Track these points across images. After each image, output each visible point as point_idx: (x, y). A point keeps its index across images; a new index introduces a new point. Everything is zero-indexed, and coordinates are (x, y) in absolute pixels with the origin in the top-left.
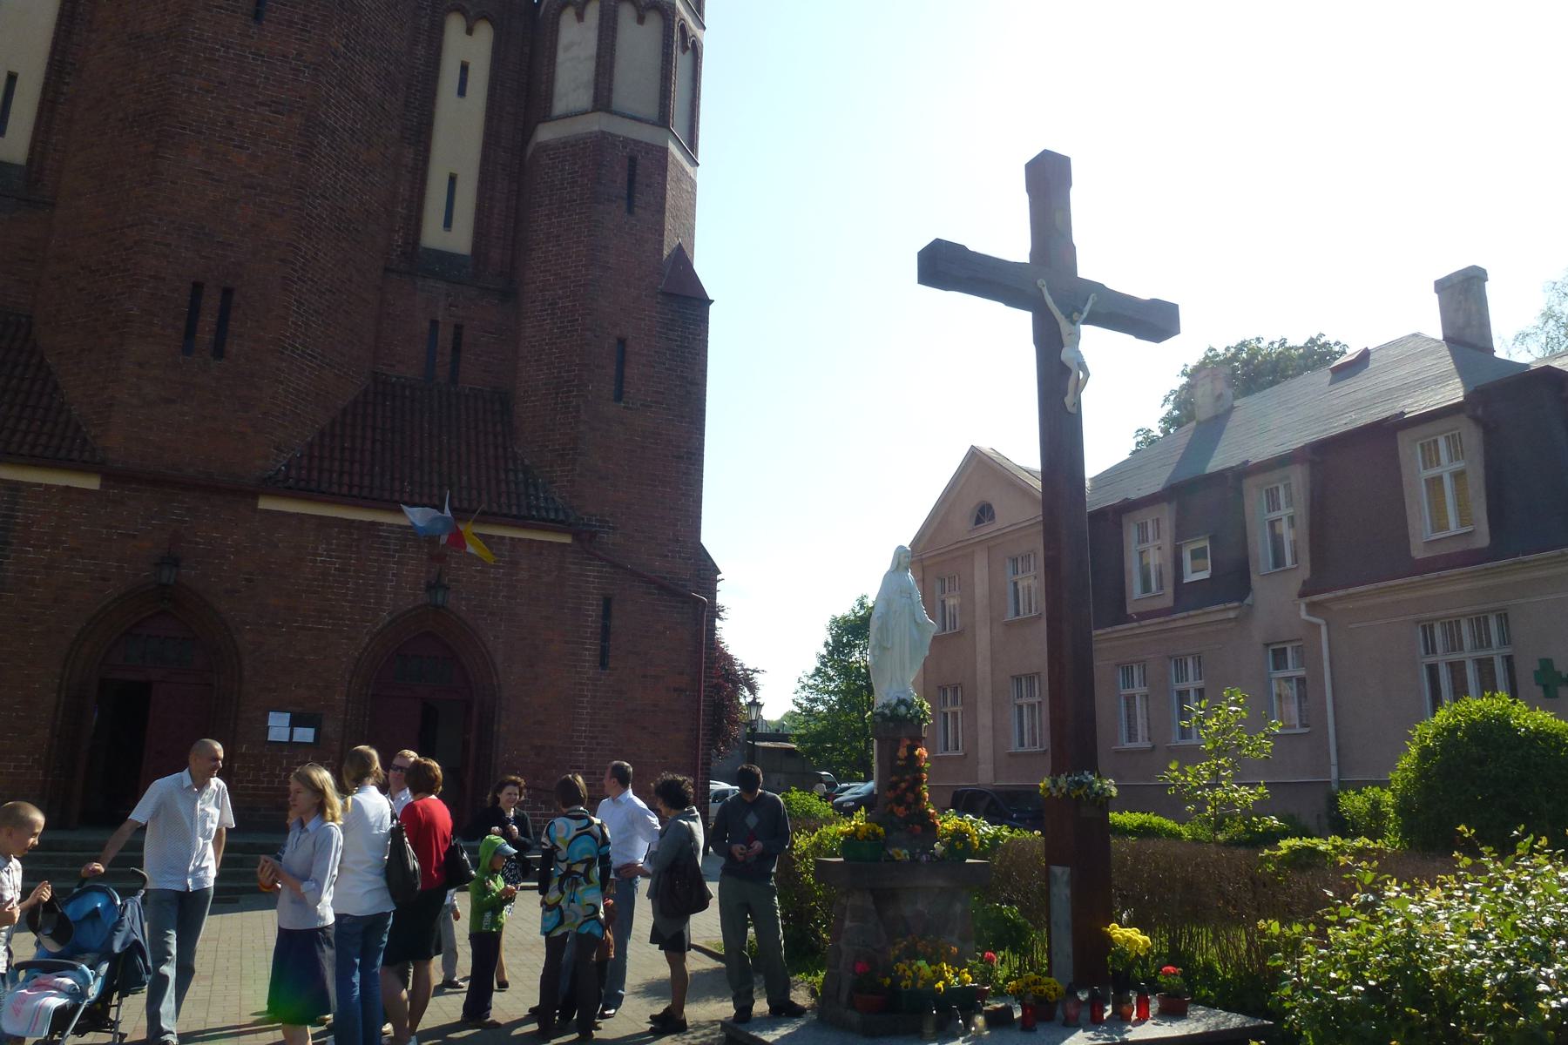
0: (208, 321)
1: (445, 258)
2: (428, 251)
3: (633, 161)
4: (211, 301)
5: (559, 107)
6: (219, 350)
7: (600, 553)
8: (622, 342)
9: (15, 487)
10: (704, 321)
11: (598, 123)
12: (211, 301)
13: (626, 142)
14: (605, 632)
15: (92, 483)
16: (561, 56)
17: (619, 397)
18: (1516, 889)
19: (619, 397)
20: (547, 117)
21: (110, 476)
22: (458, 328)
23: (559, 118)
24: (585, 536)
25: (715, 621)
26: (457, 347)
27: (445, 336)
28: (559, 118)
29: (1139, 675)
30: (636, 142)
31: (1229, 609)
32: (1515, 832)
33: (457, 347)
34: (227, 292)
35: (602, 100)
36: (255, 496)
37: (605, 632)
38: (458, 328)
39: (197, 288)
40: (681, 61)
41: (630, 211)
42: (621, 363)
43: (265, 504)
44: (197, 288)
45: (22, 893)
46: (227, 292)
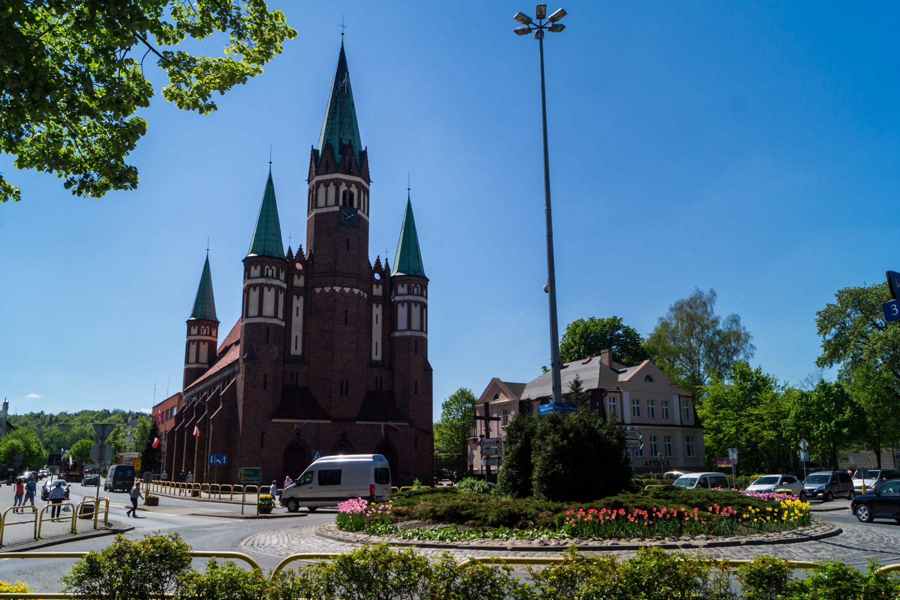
0: (344, 389)
1: (377, 362)
2: (374, 361)
3: (416, 341)
4: (345, 384)
5: (399, 328)
6: (347, 395)
8: (416, 382)
9: (319, 424)
10: (431, 374)
12: (345, 384)
15: (330, 422)
16: (399, 315)
17: (416, 393)
19: (416, 393)
21: (333, 420)
23: (399, 331)
25: (381, 276)
27: (379, 380)
28: (399, 331)
29: (204, 506)
31: (343, 490)
34: (347, 382)
39: (342, 382)
40: (425, 310)
41: (416, 352)
42: (416, 386)
43: (357, 422)
44: (342, 382)
46: (347, 382)
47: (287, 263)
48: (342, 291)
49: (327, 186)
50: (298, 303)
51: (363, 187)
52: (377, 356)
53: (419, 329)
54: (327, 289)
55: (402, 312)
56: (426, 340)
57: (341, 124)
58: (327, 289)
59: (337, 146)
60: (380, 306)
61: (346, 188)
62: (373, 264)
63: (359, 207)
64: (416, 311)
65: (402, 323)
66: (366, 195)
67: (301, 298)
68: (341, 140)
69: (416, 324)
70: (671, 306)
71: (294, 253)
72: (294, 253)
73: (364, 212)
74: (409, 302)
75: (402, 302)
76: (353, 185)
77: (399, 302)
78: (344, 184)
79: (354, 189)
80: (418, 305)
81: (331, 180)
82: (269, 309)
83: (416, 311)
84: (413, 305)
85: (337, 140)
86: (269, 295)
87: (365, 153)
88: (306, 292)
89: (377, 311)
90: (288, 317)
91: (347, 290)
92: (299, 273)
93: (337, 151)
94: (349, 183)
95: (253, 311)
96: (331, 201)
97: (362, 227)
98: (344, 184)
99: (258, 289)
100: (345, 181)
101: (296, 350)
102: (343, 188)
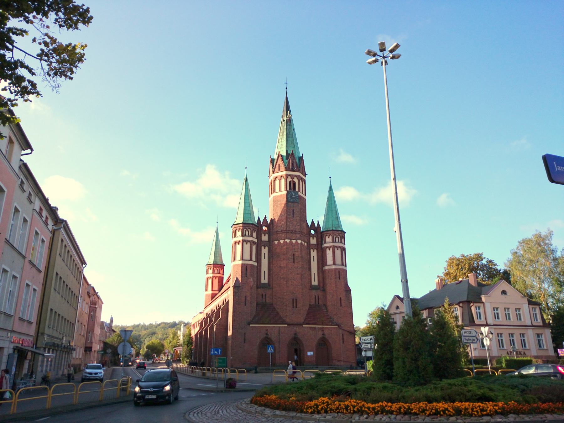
4: (295, 301)
7: (271, 260)
8: (341, 298)
11: (334, 267)
12: (295, 301)
13: (338, 269)
14: (343, 339)
15: (286, 326)
16: (327, 256)
17: (341, 306)
18: (376, 410)
19: (341, 306)
20: (326, 265)
21: (289, 324)
22: (318, 296)
24: (339, 326)
26: (318, 299)
30: (339, 269)
32: (442, 344)
33: (318, 299)
34: (296, 299)
35: (334, 264)
36: (303, 325)
37: (343, 339)
38: (318, 296)
39: (293, 299)
44: (293, 299)
45: (489, 402)
46: (296, 299)
50: (265, 251)
51: (302, 178)
54: (282, 241)
55: (329, 253)
58: (282, 241)
61: (291, 180)
66: (303, 183)
67: (267, 248)
69: (338, 261)
71: (262, 221)
72: (262, 221)
73: (303, 193)
76: (295, 178)
77: (327, 247)
79: (296, 180)
80: (339, 249)
83: (338, 252)
88: (269, 244)
89: (314, 254)
90: (259, 260)
92: (265, 232)
98: (289, 177)
99: (331, 249)
102: (289, 179)
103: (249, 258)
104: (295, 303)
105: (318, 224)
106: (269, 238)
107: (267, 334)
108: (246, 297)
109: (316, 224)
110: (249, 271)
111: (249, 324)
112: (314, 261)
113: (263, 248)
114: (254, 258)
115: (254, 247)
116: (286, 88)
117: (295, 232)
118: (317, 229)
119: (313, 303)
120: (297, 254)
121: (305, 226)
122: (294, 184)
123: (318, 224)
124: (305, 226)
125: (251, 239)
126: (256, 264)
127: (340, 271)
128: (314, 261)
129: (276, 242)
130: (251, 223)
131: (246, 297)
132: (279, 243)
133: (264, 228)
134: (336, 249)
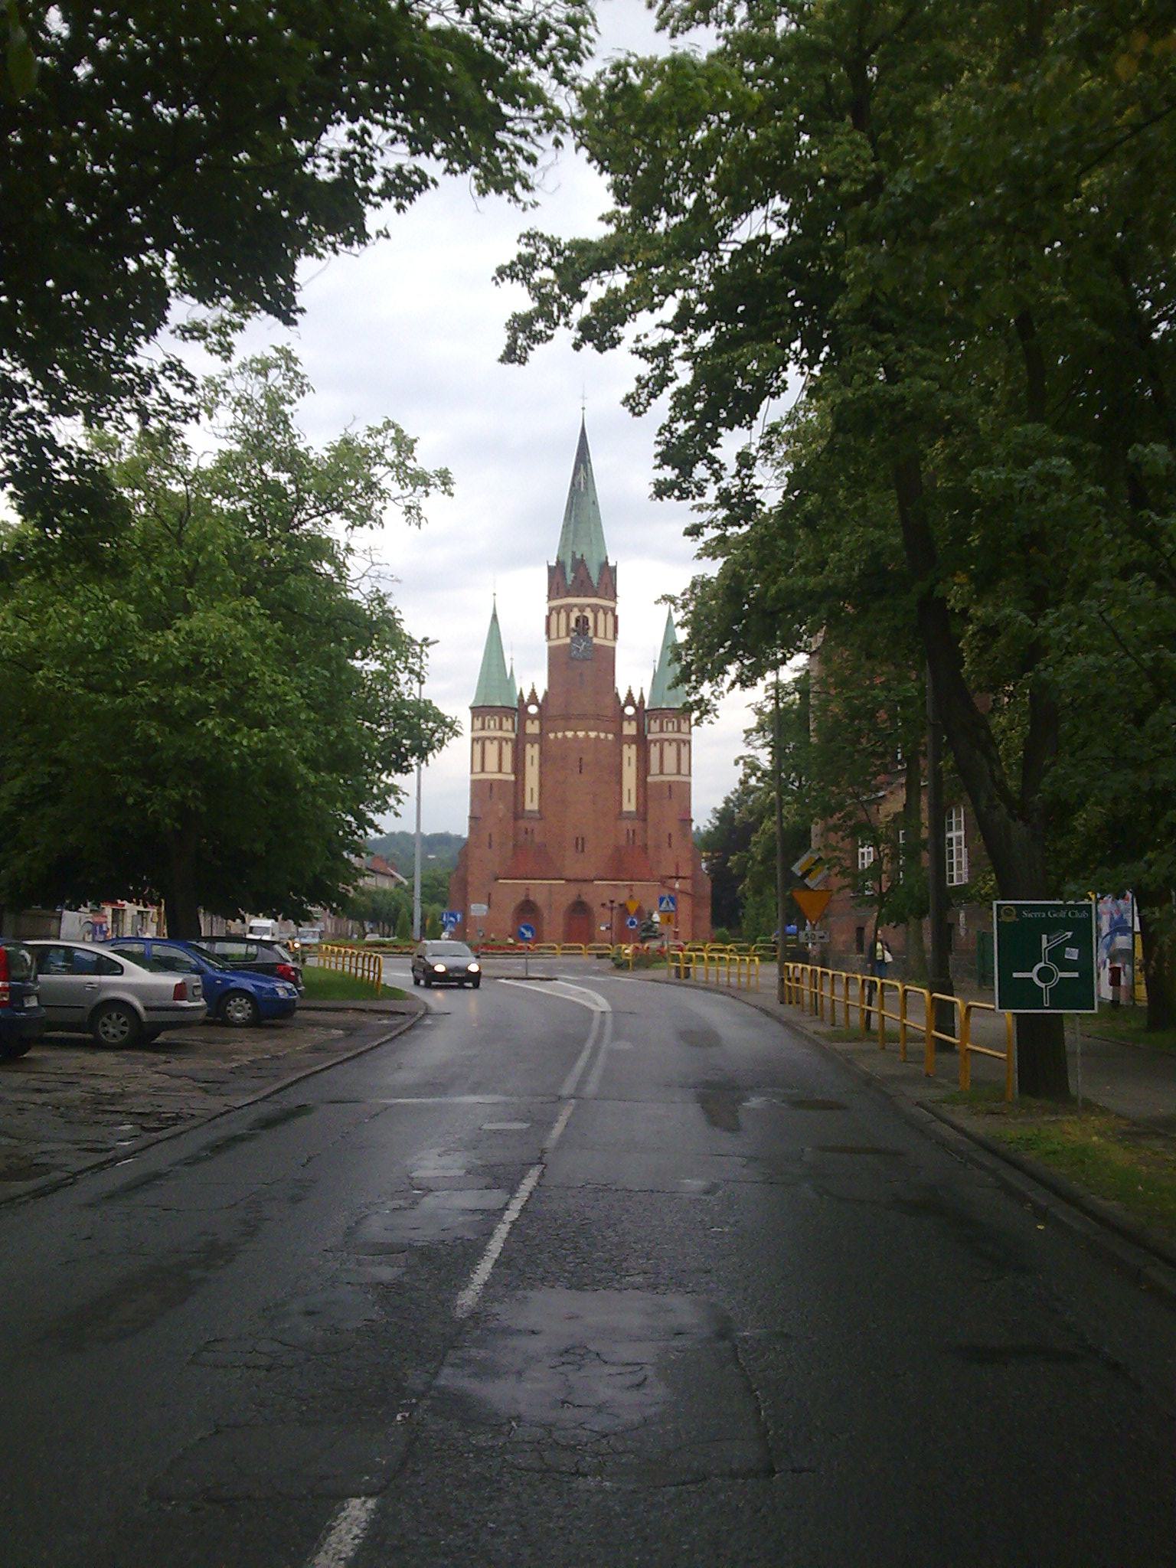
5: (652, 772)
35: (661, 773)
47: (518, 711)
48: (576, 737)
49: (558, 613)
50: (532, 752)
52: (630, 805)
53: (675, 771)
54: (560, 735)
55: (654, 751)
56: (689, 784)
57: (575, 536)
58: (560, 735)
59: (569, 563)
60: (634, 747)
61: (578, 614)
62: (623, 697)
63: (596, 635)
64: (670, 752)
65: (654, 767)
67: (536, 746)
68: (574, 553)
70: (657, 57)
71: (526, 698)
72: (526, 698)
74: (662, 741)
75: (655, 741)
76: (588, 609)
77: (652, 741)
78: (576, 609)
79: (589, 614)
81: (562, 607)
82: (492, 763)
84: (504, 744)
85: (570, 554)
86: (492, 749)
87: (614, 569)
88: (541, 738)
89: (630, 753)
90: (519, 767)
91: (581, 734)
92: (533, 717)
93: (568, 569)
94: (582, 608)
95: (478, 768)
96: (563, 633)
97: (606, 659)
98: (576, 609)
100: (576, 605)
101: (532, 804)
102: (575, 614)
103: (496, 769)
104: (580, 844)
105: (642, 696)
106: (541, 729)
107: (527, 895)
108: (490, 835)
109: (637, 699)
110: (495, 789)
111: (497, 879)
112: (532, 800)
113: (528, 746)
114: (508, 766)
115: (508, 750)
116: (583, 409)
117: (583, 717)
118: (640, 709)
119: (623, 842)
120: (587, 758)
121: (609, 701)
122: (586, 619)
123: (642, 696)
124: (609, 701)
125: (499, 734)
126: (512, 778)
127: (673, 787)
128: (532, 800)
129: (552, 736)
130: (499, 704)
131: (490, 835)
132: (556, 737)
133: (533, 709)
134: (666, 744)
